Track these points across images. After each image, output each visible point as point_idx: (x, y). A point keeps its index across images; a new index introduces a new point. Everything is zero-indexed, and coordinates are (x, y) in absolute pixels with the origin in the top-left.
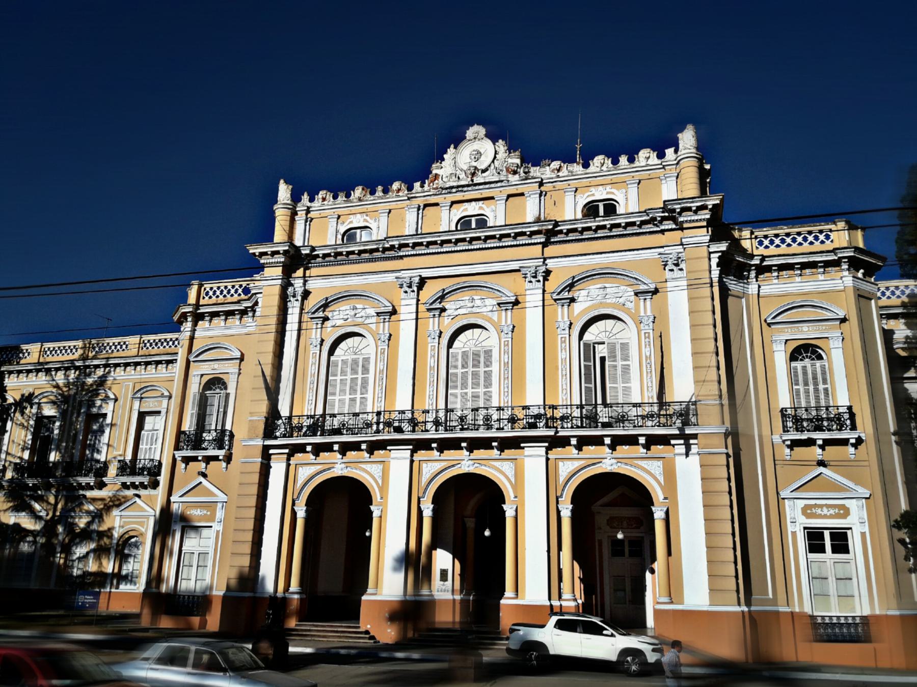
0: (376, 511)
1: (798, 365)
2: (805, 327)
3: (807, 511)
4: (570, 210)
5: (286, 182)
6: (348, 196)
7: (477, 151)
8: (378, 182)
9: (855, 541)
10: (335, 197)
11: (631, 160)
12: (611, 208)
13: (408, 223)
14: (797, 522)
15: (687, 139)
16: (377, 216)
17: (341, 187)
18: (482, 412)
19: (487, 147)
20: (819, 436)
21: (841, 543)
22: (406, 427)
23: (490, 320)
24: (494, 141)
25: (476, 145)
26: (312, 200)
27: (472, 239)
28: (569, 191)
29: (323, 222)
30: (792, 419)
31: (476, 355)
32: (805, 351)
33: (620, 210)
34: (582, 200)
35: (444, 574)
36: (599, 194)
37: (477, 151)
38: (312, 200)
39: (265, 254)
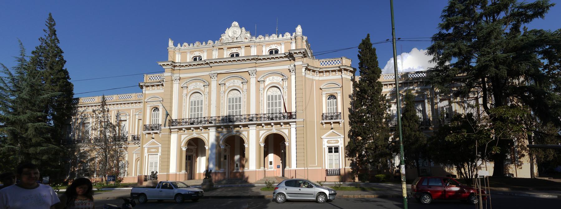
0: (246, 146)
1: (329, 101)
2: (331, 90)
3: (328, 142)
4: (265, 52)
5: (172, 40)
6: (194, 45)
7: (234, 32)
8: (203, 39)
9: (327, 150)
10: (189, 45)
11: (283, 36)
12: (237, 55)
13: (215, 55)
14: (326, 145)
15: (299, 29)
16: (207, 51)
17: (191, 41)
18: (200, 119)
19: (238, 30)
20: (332, 121)
21: (337, 150)
22: (213, 122)
23: (202, 91)
24: (241, 27)
25: (235, 29)
26: (181, 46)
27: (234, 61)
28: (265, 45)
29: (180, 53)
30: (324, 117)
31: (236, 99)
32: (332, 96)
33: (279, 53)
34: (268, 49)
35: (271, 163)
36: (273, 47)
37: (234, 32)
38: (181, 46)
39: (164, 65)
